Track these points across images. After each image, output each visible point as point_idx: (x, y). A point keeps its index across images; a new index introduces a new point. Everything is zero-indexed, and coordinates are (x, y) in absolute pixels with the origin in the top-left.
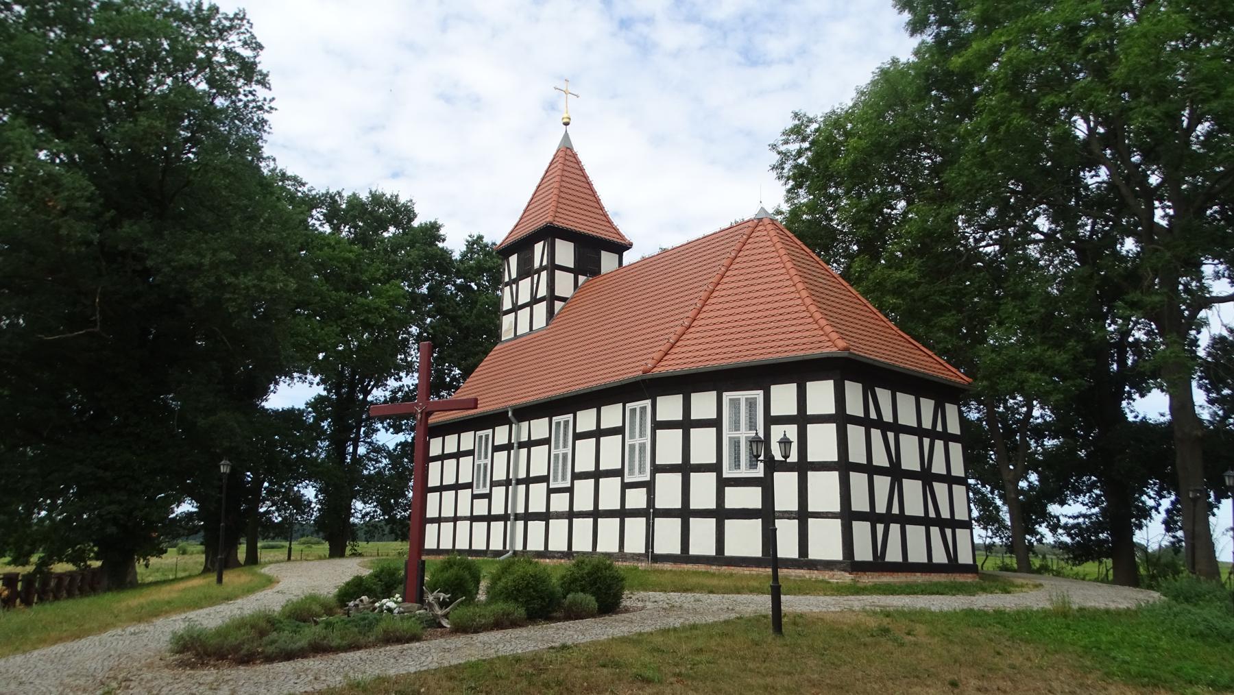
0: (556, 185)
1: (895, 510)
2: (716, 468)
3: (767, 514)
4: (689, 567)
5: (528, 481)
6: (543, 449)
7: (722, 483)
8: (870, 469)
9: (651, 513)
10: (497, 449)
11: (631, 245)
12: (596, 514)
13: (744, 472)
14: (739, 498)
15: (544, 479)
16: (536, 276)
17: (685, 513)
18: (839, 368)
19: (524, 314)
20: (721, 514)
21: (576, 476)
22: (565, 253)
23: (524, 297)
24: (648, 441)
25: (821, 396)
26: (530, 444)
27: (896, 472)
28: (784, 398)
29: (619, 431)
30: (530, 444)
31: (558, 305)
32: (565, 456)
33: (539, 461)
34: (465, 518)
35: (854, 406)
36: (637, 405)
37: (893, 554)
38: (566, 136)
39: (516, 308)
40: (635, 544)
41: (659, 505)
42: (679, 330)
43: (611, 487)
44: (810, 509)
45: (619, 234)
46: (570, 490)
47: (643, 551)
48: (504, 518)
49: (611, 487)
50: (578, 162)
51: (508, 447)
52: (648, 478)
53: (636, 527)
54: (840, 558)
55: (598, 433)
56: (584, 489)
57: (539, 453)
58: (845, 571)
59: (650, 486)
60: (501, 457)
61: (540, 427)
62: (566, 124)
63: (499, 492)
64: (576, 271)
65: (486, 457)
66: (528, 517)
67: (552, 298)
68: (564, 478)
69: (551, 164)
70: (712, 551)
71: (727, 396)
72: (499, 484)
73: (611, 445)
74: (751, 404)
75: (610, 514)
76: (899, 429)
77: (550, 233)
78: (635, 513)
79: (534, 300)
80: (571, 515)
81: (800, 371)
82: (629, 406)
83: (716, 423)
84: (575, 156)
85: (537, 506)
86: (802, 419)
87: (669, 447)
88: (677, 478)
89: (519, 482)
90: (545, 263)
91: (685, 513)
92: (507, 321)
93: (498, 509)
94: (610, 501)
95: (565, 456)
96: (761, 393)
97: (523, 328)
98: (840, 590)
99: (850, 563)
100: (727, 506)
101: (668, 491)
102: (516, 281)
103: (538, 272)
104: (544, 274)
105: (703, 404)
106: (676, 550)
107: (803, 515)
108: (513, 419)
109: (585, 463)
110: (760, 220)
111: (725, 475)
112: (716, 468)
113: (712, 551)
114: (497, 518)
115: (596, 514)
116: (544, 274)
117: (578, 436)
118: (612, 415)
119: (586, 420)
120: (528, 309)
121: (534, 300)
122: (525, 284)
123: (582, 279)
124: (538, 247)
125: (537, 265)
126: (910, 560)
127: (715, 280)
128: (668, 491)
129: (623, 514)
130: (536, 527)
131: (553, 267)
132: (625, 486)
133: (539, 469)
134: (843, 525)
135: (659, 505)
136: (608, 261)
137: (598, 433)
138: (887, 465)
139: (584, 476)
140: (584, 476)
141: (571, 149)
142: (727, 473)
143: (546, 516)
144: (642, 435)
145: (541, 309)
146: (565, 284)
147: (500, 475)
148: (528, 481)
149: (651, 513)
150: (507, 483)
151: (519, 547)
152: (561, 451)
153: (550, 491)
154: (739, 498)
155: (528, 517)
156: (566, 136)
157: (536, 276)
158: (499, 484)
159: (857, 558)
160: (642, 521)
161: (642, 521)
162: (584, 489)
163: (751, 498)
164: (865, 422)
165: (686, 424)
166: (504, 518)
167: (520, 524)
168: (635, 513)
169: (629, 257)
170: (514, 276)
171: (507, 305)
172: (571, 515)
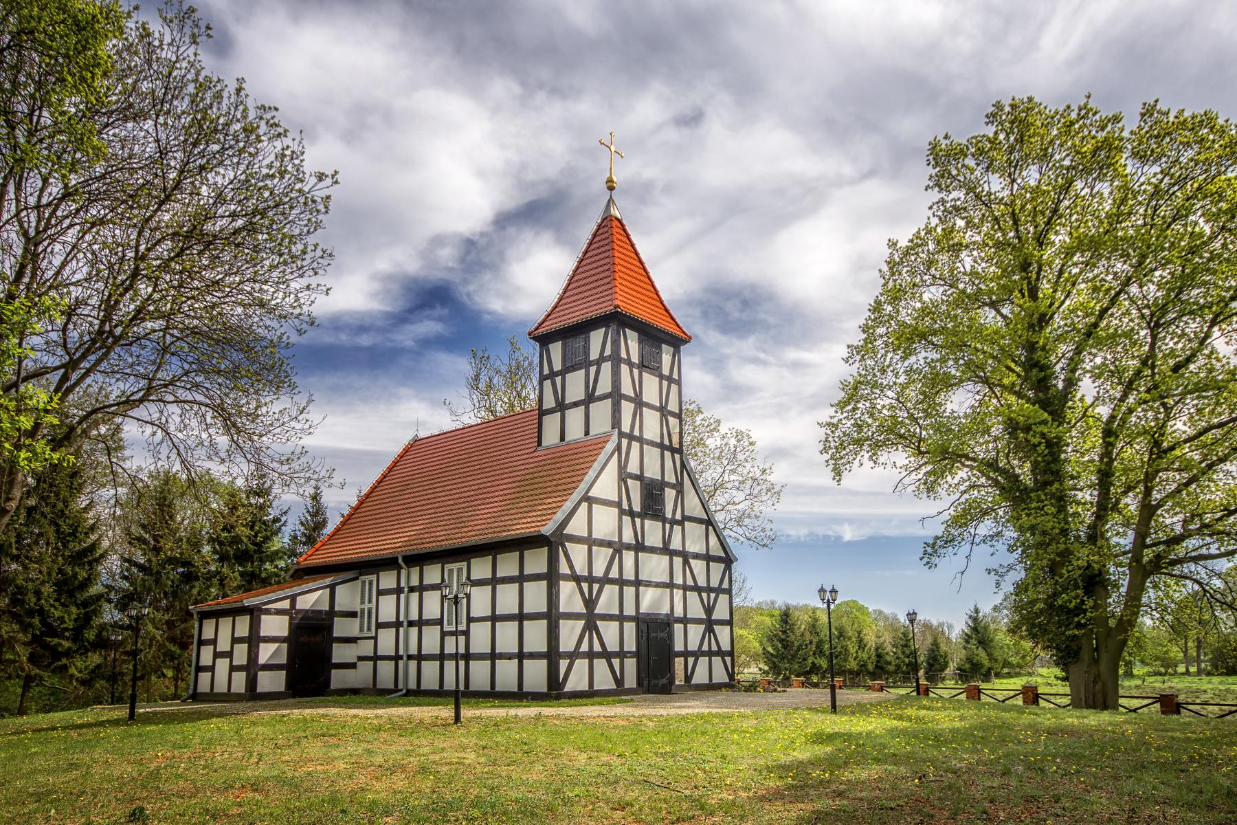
2: (440, 622)
16: (593, 370)
17: (493, 656)
21: (380, 626)
65: (370, 602)
71: (448, 567)
74: (460, 570)
79: (591, 397)
89: (411, 624)
90: (608, 352)
91: (493, 656)
101: (480, 638)
102: (563, 373)
103: (598, 363)
104: (607, 367)
112: (440, 622)
117: (380, 593)
121: (591, 397)
125: (594, 355)
138: (598, 622)
139: (387, 625)
140: (387, 625)
157: (593, 370)
167: (413, 664)
170: (557, 366)
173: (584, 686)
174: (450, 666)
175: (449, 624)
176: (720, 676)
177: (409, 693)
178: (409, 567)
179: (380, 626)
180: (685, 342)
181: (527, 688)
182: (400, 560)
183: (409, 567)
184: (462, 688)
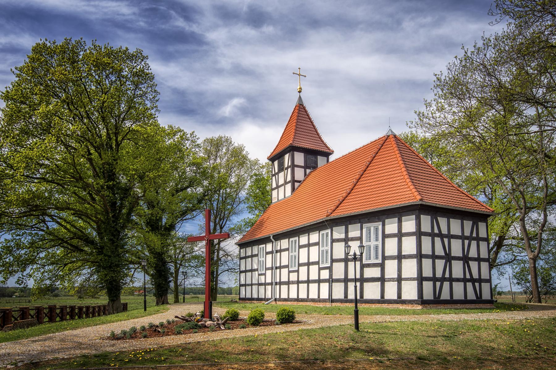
0: (294, 124)
1: (447, 275)
3: (382, 280)
4: (385, 306)
5: (280, 267)
6: (286, 253)
7: (363, 266)
8: (434, 257)
9: (331, 281)
10: (267, 253)
11: (333, 152)
12: (308, 282)
13: (373, 261)
14: (370, 273)
15: (287, 266)
16: (277, 176)
18: (419, 209)
19: (281, 189)
20: (363, 280)
21: (300, 265)
22: (300, 158)
23: (281, 182)
24: (380, 243)
25: (409, 225)
26: (281, 251)
27: (448, 258)
28: (391, 227)
29: (287, 249)
30: (281, 251)
31: (297, 185)
32: (377, 247)
33: (284, 258)
34: (255, 284)
35: (426, 226)
36: (324, 232)
37: (445, 295)
38: (300, 97)
39: (278, 187)
40: (325, 295)
41: (334, 277)
42: (344, 195)
43: (314, 269)
44: (403, 277)
45: (327, 147)
46: (298, 271)
47: (328, 298)
48: (271, 284)
49: (314, 269)
50: (306, 112)
51: (272, 252)
52: (329, 265)
53: (325, 287)
54: (416, 298)
55: (309, 245)
56: (303, 270)
57: (285, 254)
58: (418, 304)
59: (330, 269)
60: (269, 257)
61: (284, 243)
62: (300, 92)
63: (269, 273)
64: (305, 167)
65: (377, 240)
66: (281, 283)
67: (293, 181)
68: (377, 258)
69: (293, 113)
70: (395, 297)
72: (269, 269)
73: (314, 250)
74: (377, 229)
75: (314, 281)
76: (450, 237)
77: (292, 149)
78: (325, 281)
79: (286, 183)
80: (298, 282)
81: (399, 212)
82: (291, 240)
83: (360, 239)
84: (304, 108)
85: (284, 279)
86: (400, 235)
87: (339, 250)
88: (342, 264)
90: (290, 164)
91: (346, 280)
92: (274, 193)
93: (269, 280)
94: (314, 276)
95: (377, 247)
96: (381, 223)
97: (281, 197)
98: (414, 313)
99: (422, 301)
100: (365, 277)
102: (278, 173)
103: (287, 169)
104: (289, 170)
105: (354, 232)
106: (342, 297)
107: (399, 280)
108: (273, 240)
109: (303, 259)
110: (388, 136)
111: (321, 266)
113: (395, 297)
114: (269, 284)
115: (308, 282)
116: (289, 170)
117: (300, 247)
118: (314, 237)
119: (304, 240)
120: (283, 187)
121: (286, 183)
122: (281, 175)
123: (308, 171)
124: (287, 157)
126: (454, 298)
127: (363, 169)
128: (339, 270)
129: (319, 281)
130: (284, 288)
131: (293, 166)
132: (320, 269)
133: (285, 262)
134: (418, 284)
135: (334, 277)
136: (321, 161)
137: (309, 245)
141: (302, 105)
142: (365, 262)
143: (288, 283)
144: (377, 240)
145: (289, 187)
146: (299, 174)
147: (269, 265)
148: (280, 267)
149: (331, 281)
150: (272, 268)
151: (278, 297)
152: (294, 254)
153: (289, 272)
154: (370, 273)
155: (281, 283)
156: (300, 97)
158: (269, 269)
159: (425, 298)
160: (327, 284)
161: (327, 284)
162: (303, 270)
163: (375, 272)
164: (432, 235)
165: (346, 240)
166: (271, 284)
168: (325, 281)
169: (332, 158)
170: (276, 171)
171: (274, 186)
172: (298, 282)
173: (316, 297)
174: (351, 286)
175: (292, 267)
176: (471, 296)
177: (445, 302)
178: (276, 241)
179: (300, 265)
180: (331, 154)
181: (455, 298)
182: (271, 238)
183: (276, 241)
184: (358, 298)
